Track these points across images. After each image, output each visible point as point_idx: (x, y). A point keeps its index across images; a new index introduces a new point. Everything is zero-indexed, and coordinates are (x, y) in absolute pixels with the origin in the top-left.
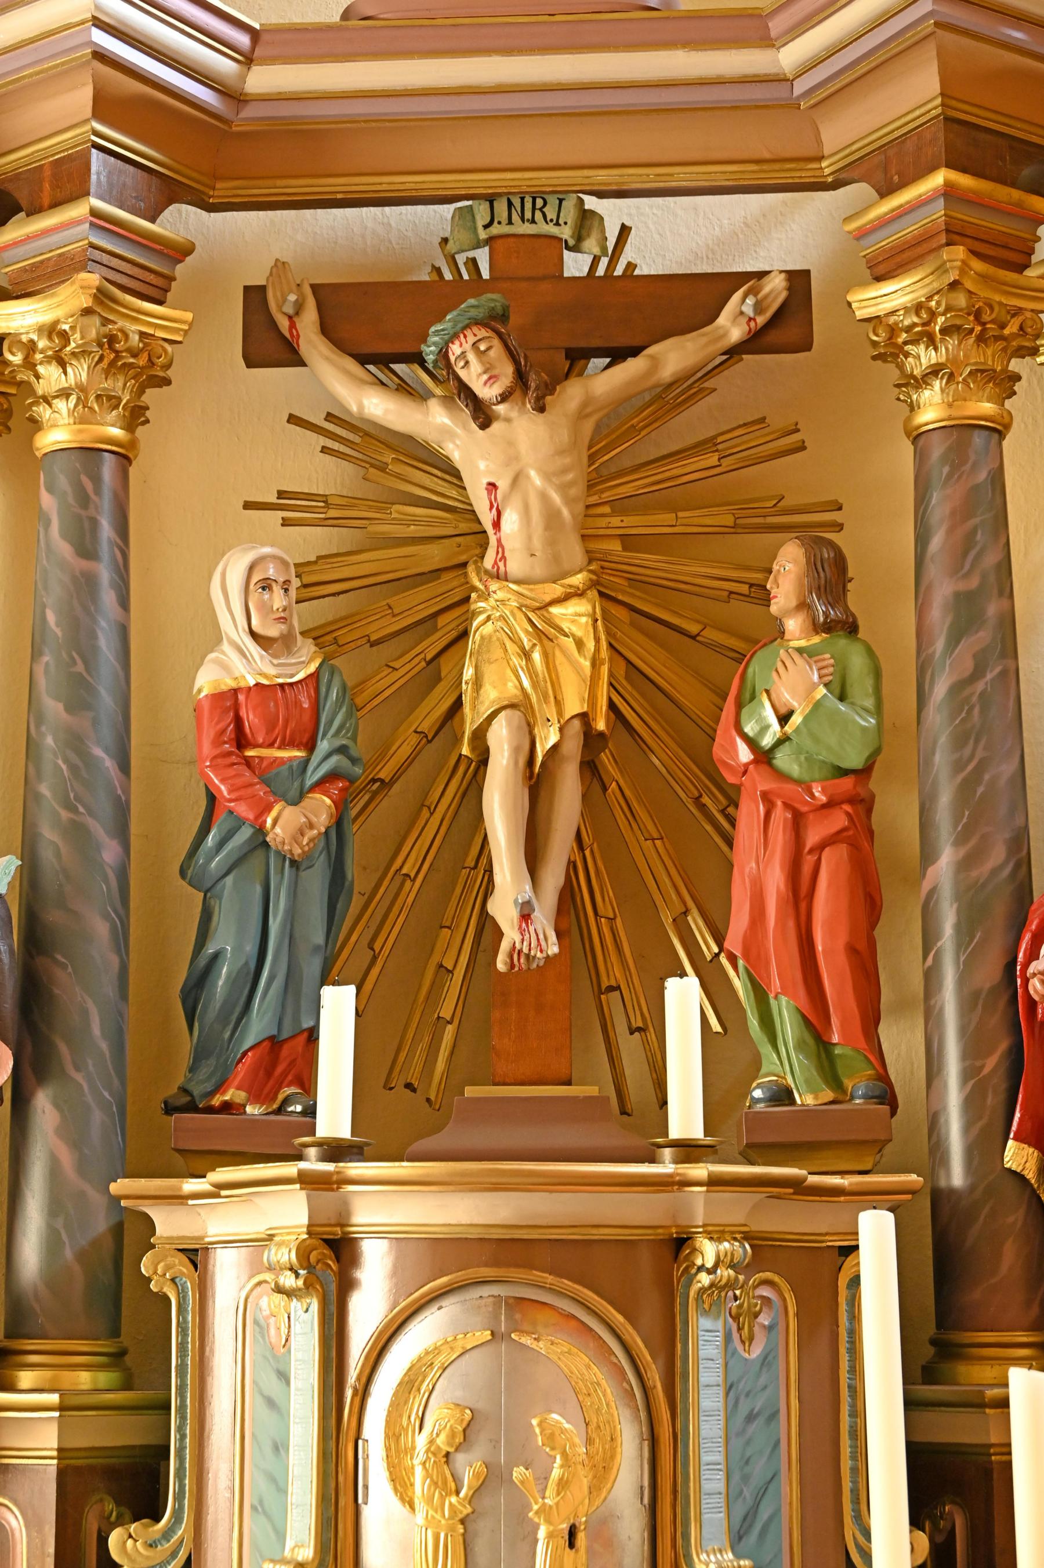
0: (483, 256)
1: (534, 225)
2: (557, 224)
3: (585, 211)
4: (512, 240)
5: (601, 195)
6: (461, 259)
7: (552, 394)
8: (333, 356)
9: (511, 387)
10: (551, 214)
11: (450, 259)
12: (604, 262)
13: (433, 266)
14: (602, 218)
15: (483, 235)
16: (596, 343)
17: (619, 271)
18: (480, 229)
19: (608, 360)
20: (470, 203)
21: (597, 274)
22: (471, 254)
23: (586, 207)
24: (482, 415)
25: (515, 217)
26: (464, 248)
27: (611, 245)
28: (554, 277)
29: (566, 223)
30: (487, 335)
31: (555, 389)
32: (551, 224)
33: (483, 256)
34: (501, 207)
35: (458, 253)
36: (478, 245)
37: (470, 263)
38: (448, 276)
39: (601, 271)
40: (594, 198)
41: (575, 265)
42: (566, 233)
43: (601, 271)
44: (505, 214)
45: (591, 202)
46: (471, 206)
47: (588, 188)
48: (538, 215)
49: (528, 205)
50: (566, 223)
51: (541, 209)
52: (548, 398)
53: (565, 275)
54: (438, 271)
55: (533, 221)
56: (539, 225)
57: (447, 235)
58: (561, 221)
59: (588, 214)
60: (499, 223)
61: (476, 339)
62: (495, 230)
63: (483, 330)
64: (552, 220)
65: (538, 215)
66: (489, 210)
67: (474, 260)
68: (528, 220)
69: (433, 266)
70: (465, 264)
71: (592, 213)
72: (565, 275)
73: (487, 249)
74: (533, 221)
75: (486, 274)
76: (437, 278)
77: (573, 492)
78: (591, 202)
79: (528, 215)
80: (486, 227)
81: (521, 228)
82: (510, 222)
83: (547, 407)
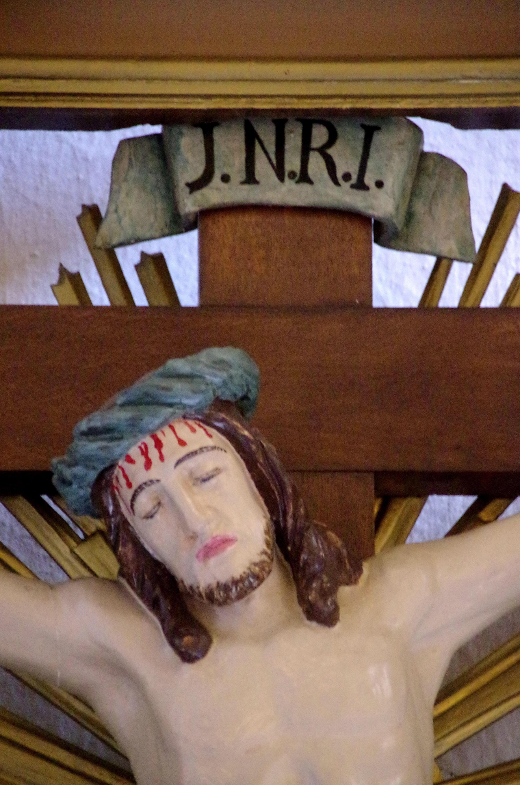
0: (183, 255)
1: (305, 187)
2: (361, 185)
3: (424, 155)
4: (251, 218)
5: (460, 119)
6: (128, 258)
7: (352, 581)
8: (140, 536)
9: (261, 564)
10: (346, 161)
11: (103, 255)
12: (460, 273)
13: (63, 271)
14: (462, 174)
15: (190, 204)
16: (450, 461)
17: (493, 298)
18: (182, 191)
19: (469, 500)
20: (157, 129)
21: (442, 304)
22: (152, 247)
23: (427, 148)
24: (183, 614)
25: (263, 167)
26: (140, 232)
27: (479, 227)
28: (351, 305)
29: (380, 184)
30: (210, 442)
31: (358, 570)
32: (346, 186)
33: (183, 255)
34: (230, 145)
35: (122, 244)
36: (178, 224)
37: (151, 268)
38: (99, 296)
39: (451, 296)
40: (445, 127)
41: (397, 279)
42: (382, 204)
43: (451, 296)
44: (239, 160)
45: (439, 137)
46: (157, 137)
47: (434, 104)
48: (316, 165)
49: (293, 141)
50: (380, 184)
51: (322, 151)
52: (345, 592)
53: (376, 304)
54: (75, 281)
55: (304, 177)
56: (318, 186)
57: (99, 195)
58: (369, 180)
59: (430, 163)
60: (225, 178)
61: (184, 451)
62: (215, 194)
63: (200, 431)
64: (347, 177)
65: (316, 165)
66: (201, 147)
67: (159, 260)
68: (292, 175)
69: (63, 271)
70: (138, 267)
71: (442, 160)
72: (376, 304)
73: (194, 235)
74: (304, 177)
75: (188, 295)
76: (73, 300)
77: (144, 503)
78: (439, 137)
79: (292, 163)
80: (194, 186)
81: (274, 191)
82: (250, 178)
83: (342, 612)
